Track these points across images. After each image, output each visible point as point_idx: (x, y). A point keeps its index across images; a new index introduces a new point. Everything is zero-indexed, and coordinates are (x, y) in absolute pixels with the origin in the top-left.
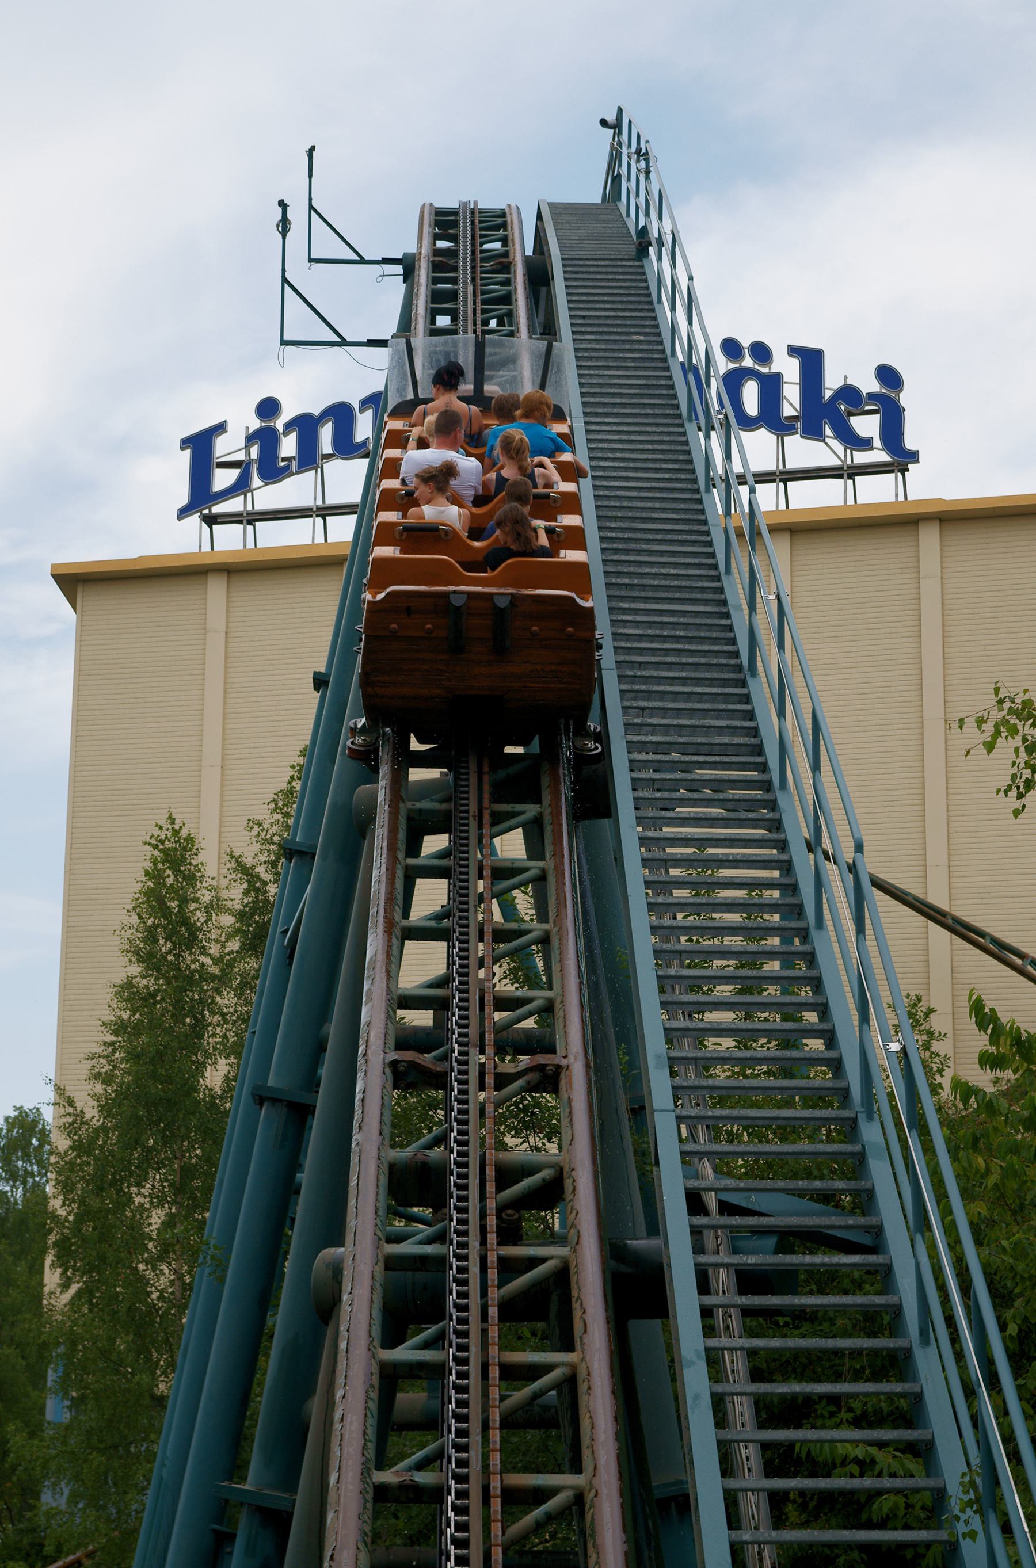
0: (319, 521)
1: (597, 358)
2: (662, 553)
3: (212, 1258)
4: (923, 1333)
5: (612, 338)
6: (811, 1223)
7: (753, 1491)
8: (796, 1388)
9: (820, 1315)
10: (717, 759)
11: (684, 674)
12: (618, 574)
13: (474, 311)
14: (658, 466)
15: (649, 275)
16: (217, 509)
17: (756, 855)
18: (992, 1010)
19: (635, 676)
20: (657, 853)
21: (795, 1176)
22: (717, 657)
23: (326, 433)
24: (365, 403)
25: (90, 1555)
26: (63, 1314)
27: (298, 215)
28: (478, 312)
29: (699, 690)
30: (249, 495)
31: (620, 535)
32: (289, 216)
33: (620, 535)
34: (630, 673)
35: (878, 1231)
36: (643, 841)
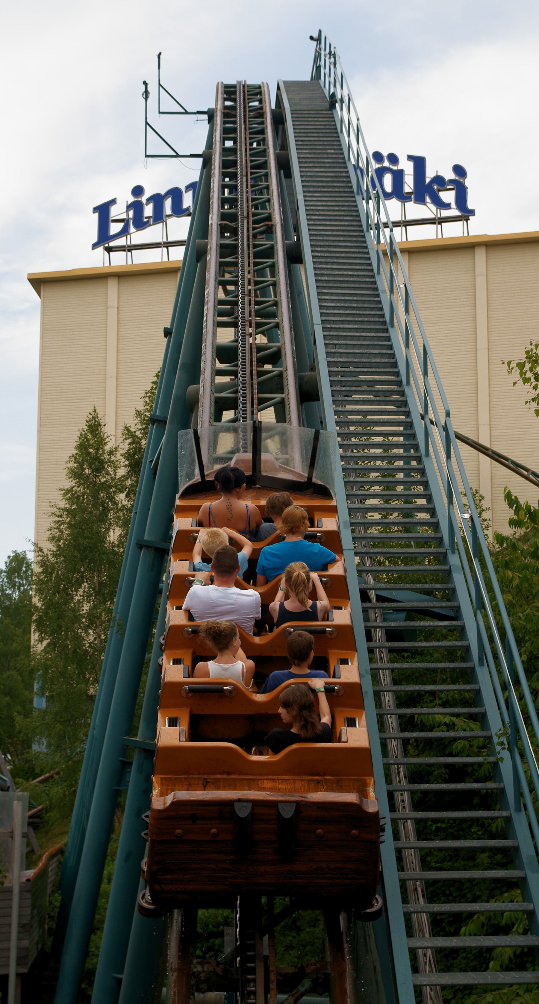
0: (165, 249)
1: (310, 162)
2: (344, 264)
3: (118, 625)
4: (480, 659)
5: (317, 151)
6: (424, 606)
7: (394, 738)
8: (417, 688)
9: (425, 652)
10: (374, 370)
11: (356, 326)
12: (322, 275)
13: (245, 138)
14: (342, 218)
15: (336, 118)
16: (112, 244)
17: (394, 419)
18: (516, 497)
19: (331, 328)
20: (342, 418)
21: (413, 582)
22: (373, 317)
23: (168, 204)
24: (188, 188)
25: (58, 773)
26: (40, 654)
27: (153, 89)
28: (248, 139)
29: (364, 334)
30: (128, 236)
31: (322, 254)
32: (149, 89)
33: (322, 254)
34: (328, 326)
35: (458, 609)
36: (336, 412)
